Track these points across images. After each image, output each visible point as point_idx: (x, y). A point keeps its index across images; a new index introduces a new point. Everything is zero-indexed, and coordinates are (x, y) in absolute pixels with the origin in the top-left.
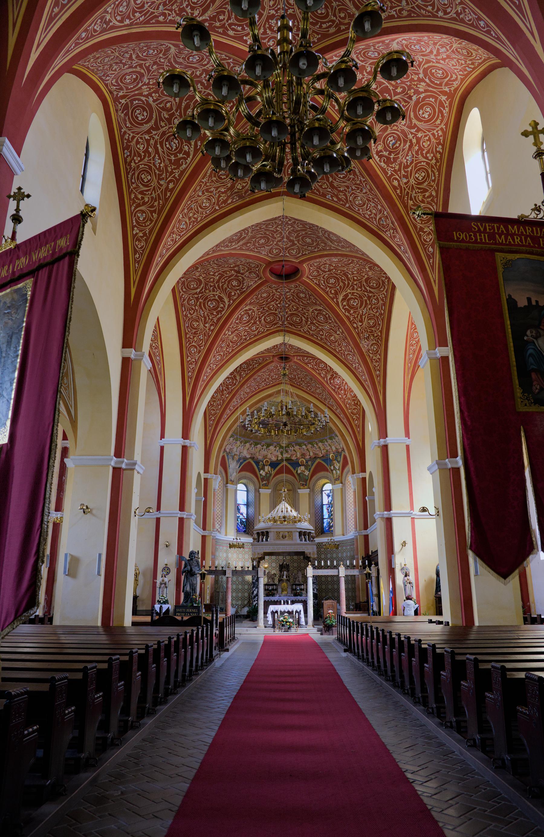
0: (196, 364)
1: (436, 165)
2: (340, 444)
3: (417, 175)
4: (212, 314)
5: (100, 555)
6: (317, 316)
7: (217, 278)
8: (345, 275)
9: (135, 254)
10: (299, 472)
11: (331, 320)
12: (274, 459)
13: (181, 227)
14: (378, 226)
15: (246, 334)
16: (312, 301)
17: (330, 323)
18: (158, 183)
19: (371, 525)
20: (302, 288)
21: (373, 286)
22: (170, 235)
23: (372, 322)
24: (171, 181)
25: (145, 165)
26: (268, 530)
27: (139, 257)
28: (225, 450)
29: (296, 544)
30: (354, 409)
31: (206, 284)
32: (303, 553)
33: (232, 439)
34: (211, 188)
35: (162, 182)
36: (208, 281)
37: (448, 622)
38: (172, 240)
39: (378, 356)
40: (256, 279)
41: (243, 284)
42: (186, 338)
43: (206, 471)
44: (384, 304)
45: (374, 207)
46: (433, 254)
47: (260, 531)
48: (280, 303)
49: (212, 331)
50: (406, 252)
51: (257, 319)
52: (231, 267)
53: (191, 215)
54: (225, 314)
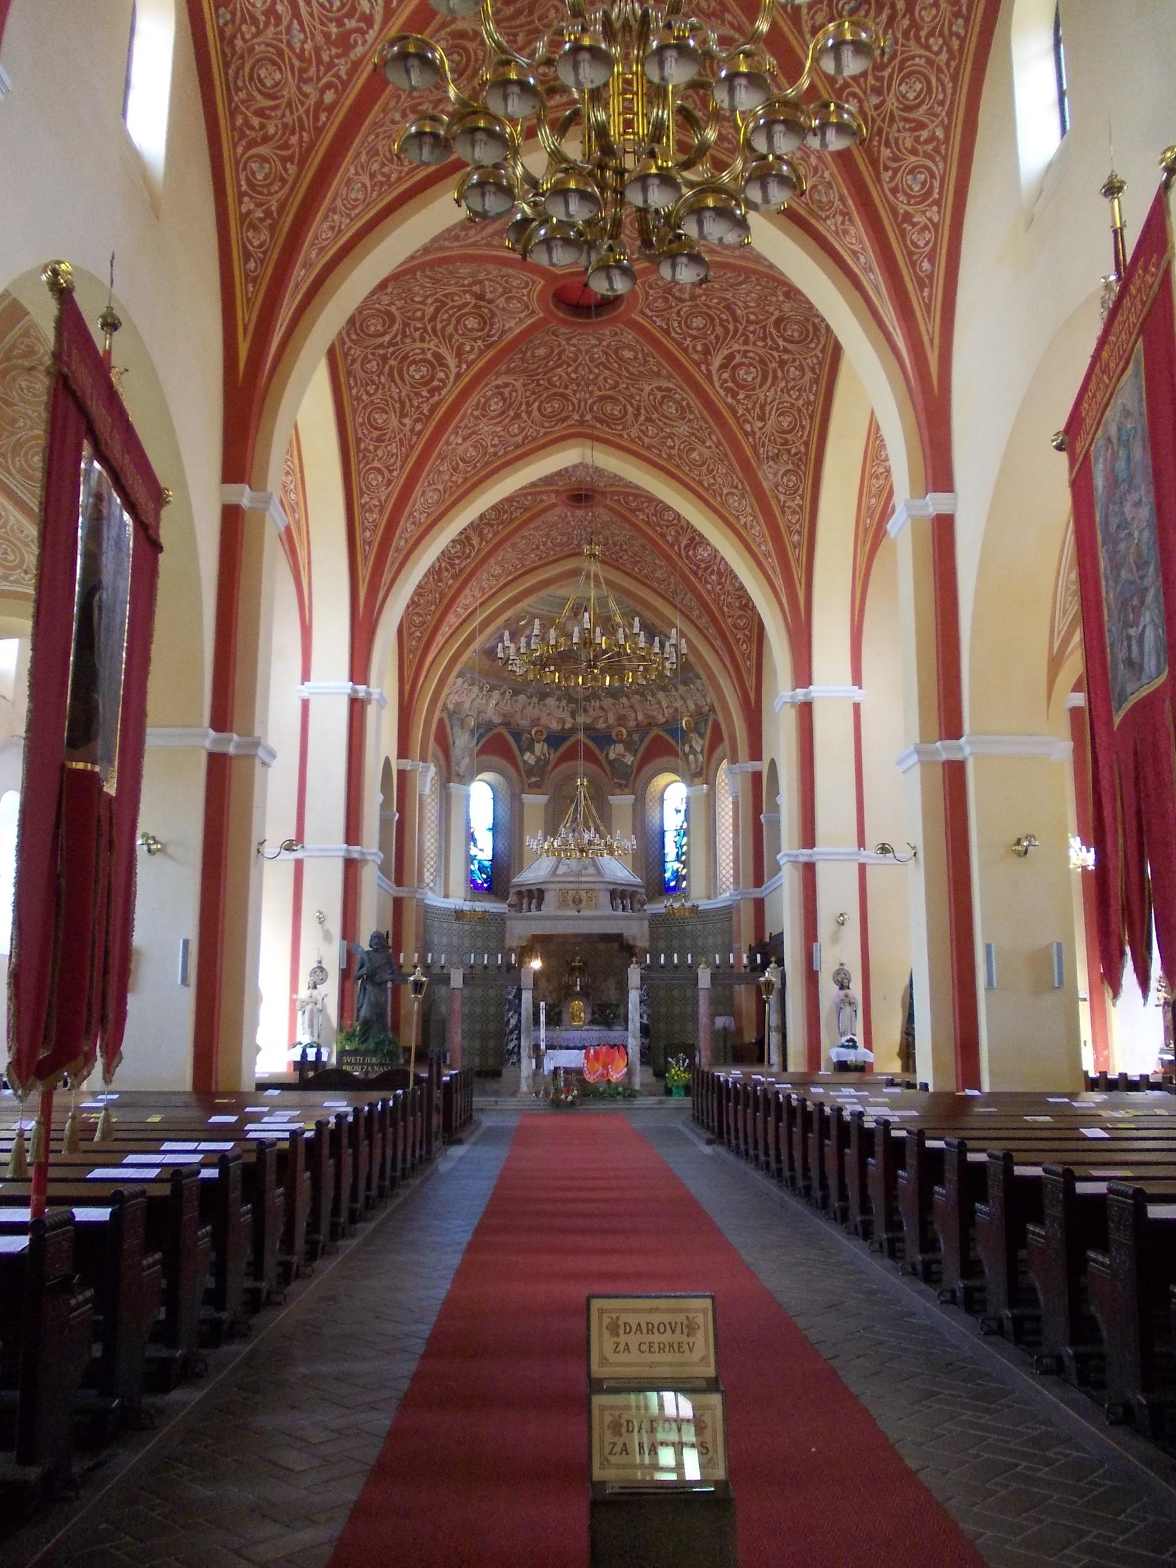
0: (381, 512)
1: (948, 64)
2: (704, 696)
3: (903, 88)
4: (418, 394)
5: (186, 943)
6: (661, 404)
7: (432, 309)
8: (729, 308)
9: (247, 260)
10: (612, 756)
11: (692, 412)
12: (555, 726)
13: (353, 196)
14: (807, 204)
15: (496, 441)
16: (651, 370)
17: (690, 421)
18: (299, 89)
19: (769, 879)
20: (629, 336)
21: (792, 336)
22: (326, 217)
23: (786, 422)
24: (329, 86)
25: (267, 45)
26: (543, 887)
27: (256, 268)
28: (445, 706)
29: (601, 918)
30: (740, 617)
31: (405, 325)
32: (618, 938)
33: (460, 681)
34: (420, 104)
35: (307, 89)
36: (409, 318)
37: (926, 1085)
38: (332, 228)
39: (798, 501)
40: (522, 315)
41: (492, 325)
42: (358, 450)
43: (403, 752)
44: (816, 381)
45: (802, 158)
46: (930, 277)
47: (523, 889)
48: (575, 371)
49: (419, 434)
50: (871, 270)
51: (523, 407)
52: (464, 286)
53: (375, 167)
54: (449, 395)
